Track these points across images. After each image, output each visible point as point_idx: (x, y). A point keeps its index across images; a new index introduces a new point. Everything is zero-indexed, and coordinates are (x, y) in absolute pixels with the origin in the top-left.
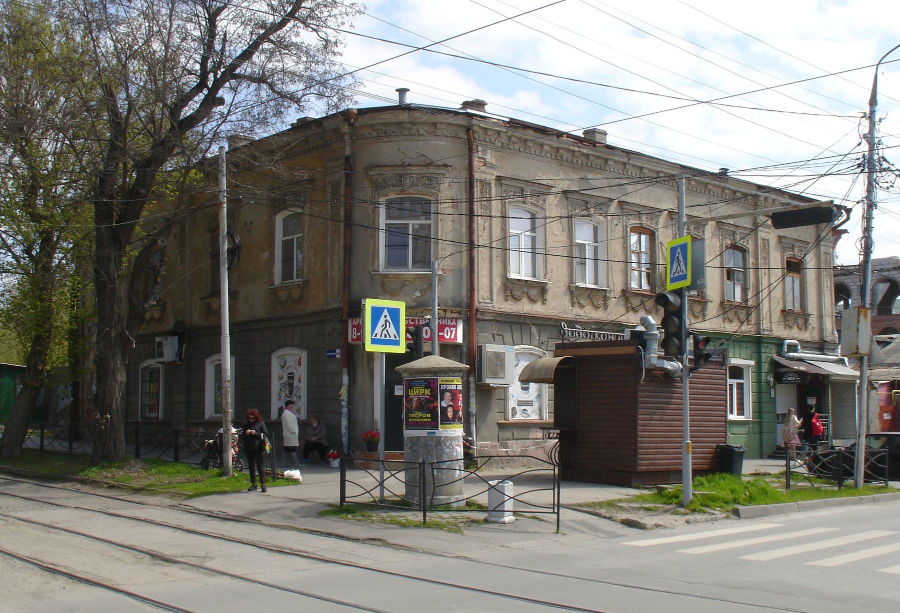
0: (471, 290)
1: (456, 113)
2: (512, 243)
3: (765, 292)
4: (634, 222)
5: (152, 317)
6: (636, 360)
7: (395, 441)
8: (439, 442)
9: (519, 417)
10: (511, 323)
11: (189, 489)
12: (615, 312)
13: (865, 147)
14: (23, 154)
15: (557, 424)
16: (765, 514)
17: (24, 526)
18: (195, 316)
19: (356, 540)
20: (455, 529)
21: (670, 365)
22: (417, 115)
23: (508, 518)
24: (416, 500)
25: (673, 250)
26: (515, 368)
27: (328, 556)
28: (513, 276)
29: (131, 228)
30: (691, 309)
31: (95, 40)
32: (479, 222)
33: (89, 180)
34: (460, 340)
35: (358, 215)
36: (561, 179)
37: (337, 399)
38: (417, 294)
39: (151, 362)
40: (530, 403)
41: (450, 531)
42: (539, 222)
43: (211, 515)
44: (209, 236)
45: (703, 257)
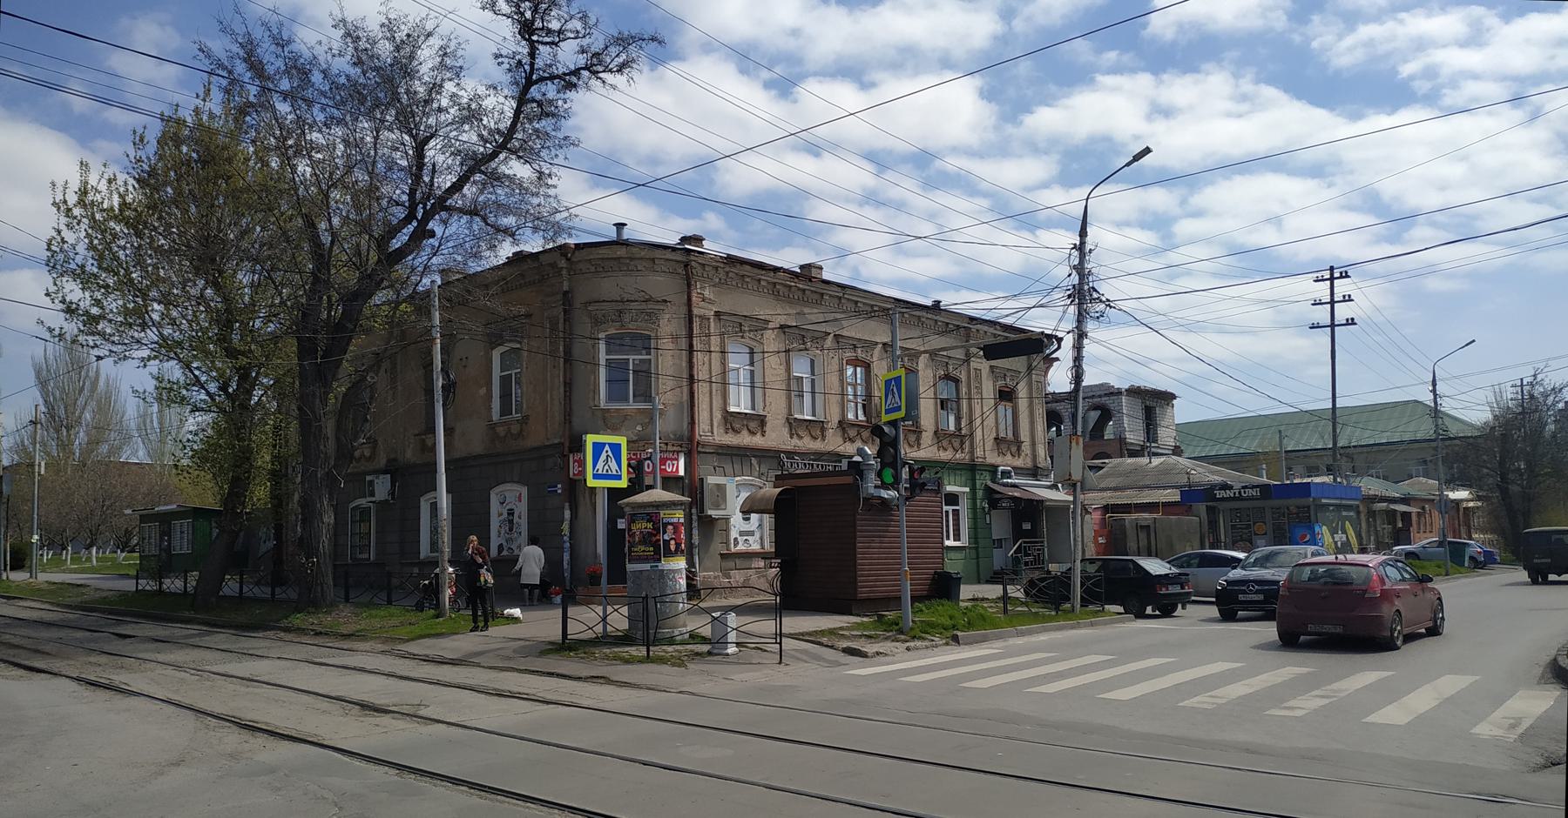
0: (692, 423)
1: (673, 249)
2: (731, 378)
3: (978, 421)
4: (849, 354)
5: (363, 455)
6: (854, 489)
7: (617, 574)
8: (662, 575)
9: (741, 547)
10: (731, 455)
11: (403, 632)
12: (833, 442)
13: (1075, 279)
14: (216, 286)
15: (777, 554)
16: (984, 639)
17: (220, 681)
18: (409, 454)
19: (579, 679)
20: (678, 662)
21: (885, 494)
22: (635, 250)
23: (732, 649)
24: (639, 635)
25: (888, 383)
26: (736, 499)
27: (549, 697)
28: (732, 409)
29: (338, 364)
30: (906, 438)
31: (294, 168)
32: (699, 357)
33: (290, 314)
34: (682, 473)
35: (577, 351)
36: (778, 313)
37: (560, 533)
38: (639, 428)
39: (362, 502)
40: (751, 533)
41: (673, 665)
42: (757, 357)
43: (427, 660)
44: (421, 372)
45: (917, 388)
